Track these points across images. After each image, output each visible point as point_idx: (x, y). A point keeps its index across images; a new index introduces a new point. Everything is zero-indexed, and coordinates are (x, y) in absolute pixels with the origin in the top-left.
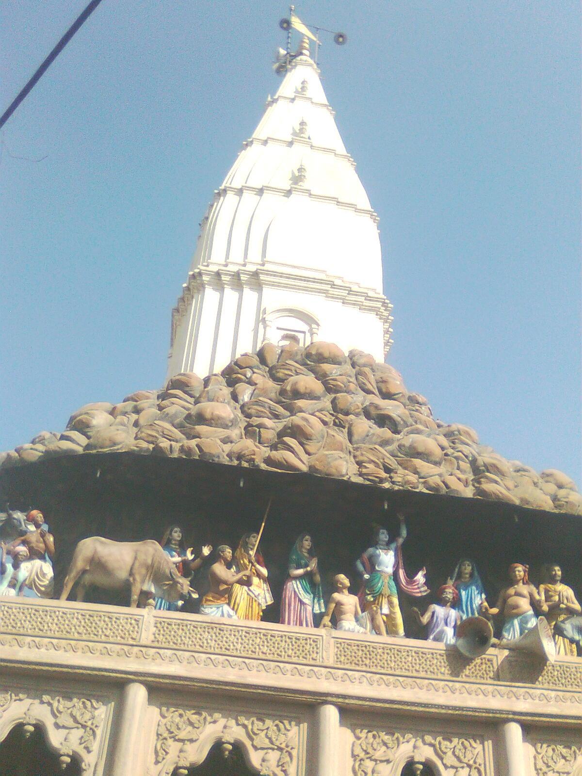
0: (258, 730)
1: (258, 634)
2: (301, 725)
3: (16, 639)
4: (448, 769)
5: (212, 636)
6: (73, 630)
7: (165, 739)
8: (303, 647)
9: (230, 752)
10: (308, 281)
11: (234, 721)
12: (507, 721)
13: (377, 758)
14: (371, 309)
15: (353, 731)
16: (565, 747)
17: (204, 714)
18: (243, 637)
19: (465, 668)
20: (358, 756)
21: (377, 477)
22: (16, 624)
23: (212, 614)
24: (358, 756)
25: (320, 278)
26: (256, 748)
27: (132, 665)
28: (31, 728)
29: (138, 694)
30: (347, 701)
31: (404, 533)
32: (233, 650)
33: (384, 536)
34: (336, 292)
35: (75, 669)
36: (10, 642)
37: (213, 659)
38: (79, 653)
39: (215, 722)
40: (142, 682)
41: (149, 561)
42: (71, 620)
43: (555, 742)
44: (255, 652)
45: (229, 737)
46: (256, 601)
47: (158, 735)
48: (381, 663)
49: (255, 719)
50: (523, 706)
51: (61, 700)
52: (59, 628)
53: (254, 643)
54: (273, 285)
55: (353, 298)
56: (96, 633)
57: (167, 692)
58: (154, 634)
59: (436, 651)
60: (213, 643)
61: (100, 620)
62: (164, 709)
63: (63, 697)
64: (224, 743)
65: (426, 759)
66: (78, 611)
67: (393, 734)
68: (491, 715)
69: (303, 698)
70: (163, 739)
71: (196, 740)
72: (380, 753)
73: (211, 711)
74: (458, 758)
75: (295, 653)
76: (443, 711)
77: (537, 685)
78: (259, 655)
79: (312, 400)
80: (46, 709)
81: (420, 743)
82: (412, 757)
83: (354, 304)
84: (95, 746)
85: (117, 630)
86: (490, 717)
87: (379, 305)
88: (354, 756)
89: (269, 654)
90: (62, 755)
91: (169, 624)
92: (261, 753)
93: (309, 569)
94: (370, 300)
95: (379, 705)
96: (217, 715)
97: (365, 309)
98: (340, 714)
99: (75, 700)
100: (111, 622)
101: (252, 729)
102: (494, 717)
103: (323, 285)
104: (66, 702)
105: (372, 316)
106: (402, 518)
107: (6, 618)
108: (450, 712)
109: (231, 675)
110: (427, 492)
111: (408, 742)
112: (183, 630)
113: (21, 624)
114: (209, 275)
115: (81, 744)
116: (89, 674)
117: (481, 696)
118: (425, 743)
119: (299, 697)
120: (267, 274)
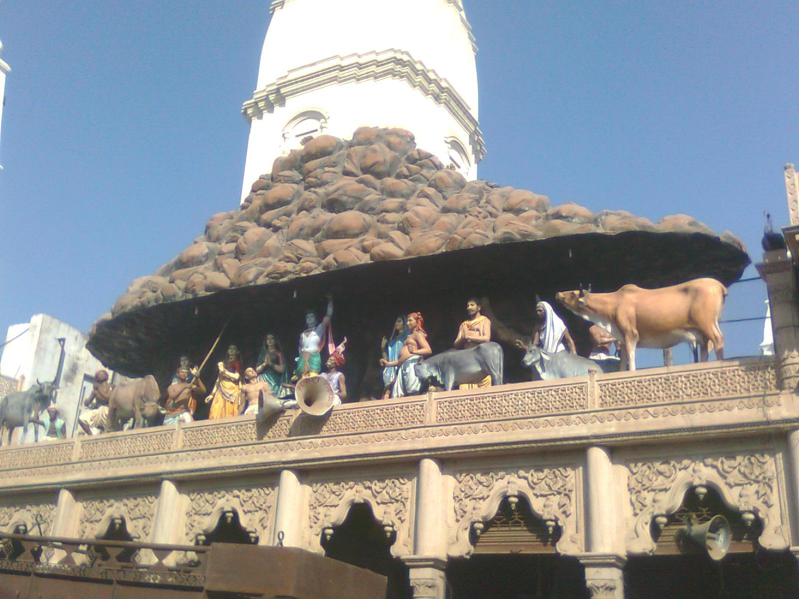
0: (729, 467)
1: (736, 372)
2: (777, 456)
3: (500, 425)
4: (733, 488)
5: (658, 387)
6: (681, 393)
7: (639, 492)
8: (702, 383)
9: (517, 504)
10: (319, 75)
11: (702, 464)
12: (163, 479)
13: (655, 488)
14: (385, 74)
15: (455, 477)
16: (482, 475)
17: (342, 484)
18: (636, 387)
19: (268, 431)
20: (634, 489)
21: (277, 273)
22: (624, 398)
23: (170, 423)
24: (634, 489)
25: (327, 68)
26: (537, 496)
27: (59, 479)
28: (515, 500)
29: (598, 456)
30: (122, 480)
31: (330, 310)
32: (628, 401)
33: (310, 319)
34: (346, 73)
35: (589, 439)
36: (718, 408)
37: (549, 420)
38: (510, 431)
39: (111, 506)
40: (67, 488)
41: (143, 393)
42: (648, 387)
43: (475, 472)
44: (707, 394)
45: (512, 490)
46: (228, 401)
47: (630, 490)
48: (647, 395)
49: (376, 481)
50: (292, 456)
51: (724, 460)
52: (613, 399)
53: (675, 388)
54: (293, 94)
55: (364, 71)
56: (622, 400)
57: (452, 461)
58: (601, 397)
59: (489, 395)
60: (661, 394)
61: (548, 395)
62: (632, 465)
63: (726, 458)
64: (509, 496)
65: (707, 481)
66: (575, 385)
67: (669, 463)
68: (267, 467)
69: (150, 479)
70: (636, 493)
71: (669, 489)
72: (659, 482)
73: (496, 470)
74: (744, 475)
75: (667, 394)
76: (235, 470)
77: (322, 434)
78: (683, 398)
79: (282, 206)
80: (523, 483)
81: (230, 497)
82: (692, 483)
83: (368, 77)
84: (774, 498)
85: (565, 401)
86: (267, 469)
87: (391, 66)
88: (630, 490)
89: (538, 410)
90: (386, 525)
91: (493, 398)
92: (737, 490)
93: (264, 364)
94: (383, 65)
95: (316, 463)
96: (686, 462)
97: (380, 76)
98: (439, 466)
99: (386, 481)
100: (558, 395)
101: (723, 469)
102: (270, 468)
103: (321, 76)
104: (380, 484)
105: (389, 80)
106: (330, 297)
107: (562, 400)
108: (240, 470)
109: (679, 421)
110: (209, 293)
111: (502, 478)
112: (627, 387)
113: (629, 397)
114: (251, 107)
115: (758, 499)
116: (552, 446)
117: (533, 429)
118: (706, 465)
119: (146, 479)
120: (286, 86)
